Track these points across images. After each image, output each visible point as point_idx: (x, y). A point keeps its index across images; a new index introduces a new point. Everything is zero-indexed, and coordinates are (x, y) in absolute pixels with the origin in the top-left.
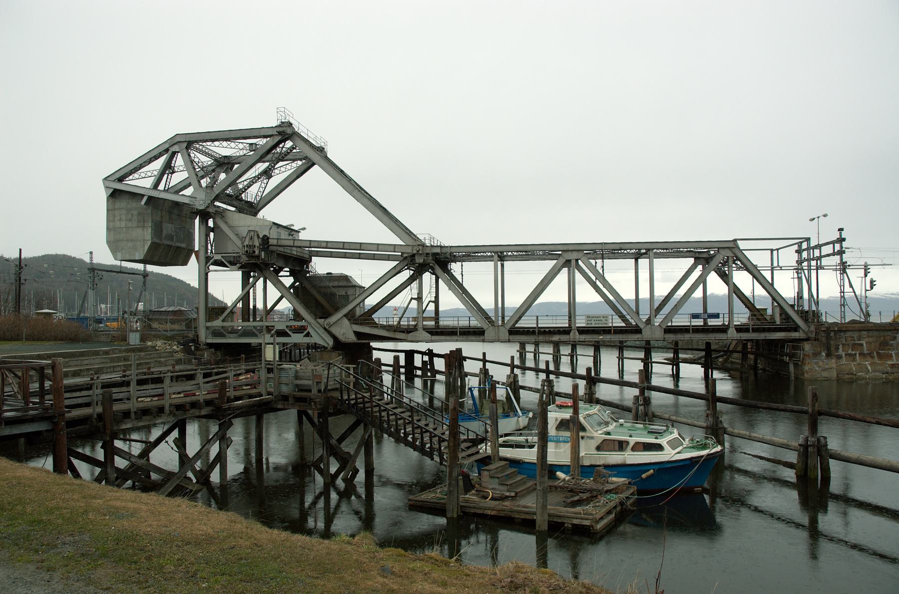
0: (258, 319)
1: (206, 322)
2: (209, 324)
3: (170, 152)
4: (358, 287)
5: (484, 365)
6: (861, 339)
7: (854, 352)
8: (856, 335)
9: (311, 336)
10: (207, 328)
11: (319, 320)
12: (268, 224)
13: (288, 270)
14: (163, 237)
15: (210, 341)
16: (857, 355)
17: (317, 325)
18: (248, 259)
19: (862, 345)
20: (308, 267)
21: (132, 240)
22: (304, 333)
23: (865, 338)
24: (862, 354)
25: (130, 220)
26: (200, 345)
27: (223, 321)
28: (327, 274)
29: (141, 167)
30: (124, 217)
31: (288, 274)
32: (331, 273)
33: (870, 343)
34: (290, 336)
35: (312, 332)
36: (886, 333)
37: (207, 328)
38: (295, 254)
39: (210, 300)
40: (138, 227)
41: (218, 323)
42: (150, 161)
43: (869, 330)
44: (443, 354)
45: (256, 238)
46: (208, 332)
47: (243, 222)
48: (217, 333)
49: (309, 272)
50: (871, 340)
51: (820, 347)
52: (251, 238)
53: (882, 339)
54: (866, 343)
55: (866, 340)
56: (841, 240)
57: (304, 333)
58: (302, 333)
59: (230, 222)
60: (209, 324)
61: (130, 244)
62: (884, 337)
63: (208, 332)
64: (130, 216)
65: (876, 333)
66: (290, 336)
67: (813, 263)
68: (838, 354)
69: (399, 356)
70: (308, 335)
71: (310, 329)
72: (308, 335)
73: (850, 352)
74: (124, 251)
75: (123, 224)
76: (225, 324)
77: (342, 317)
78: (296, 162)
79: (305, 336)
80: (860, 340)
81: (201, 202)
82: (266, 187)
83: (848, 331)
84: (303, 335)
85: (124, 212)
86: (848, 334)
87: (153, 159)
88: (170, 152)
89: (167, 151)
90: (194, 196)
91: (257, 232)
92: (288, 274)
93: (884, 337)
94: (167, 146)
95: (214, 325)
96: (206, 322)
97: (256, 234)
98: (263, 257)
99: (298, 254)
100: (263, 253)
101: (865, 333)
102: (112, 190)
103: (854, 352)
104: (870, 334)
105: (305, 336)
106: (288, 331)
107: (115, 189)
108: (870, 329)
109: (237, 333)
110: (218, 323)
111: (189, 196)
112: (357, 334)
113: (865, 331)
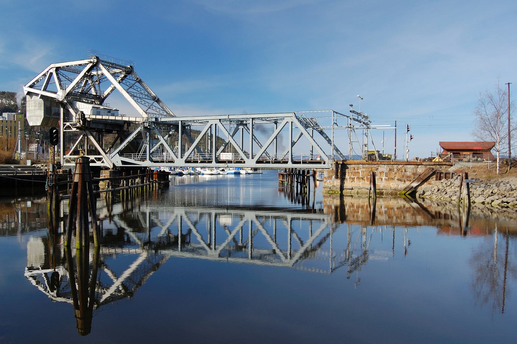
0: (13, 103)
6: (359, 169)
7: (354, 177)
8: (356, 166)
9: (104, 163)
10: (64, 158)
14: (52, 114)
16: (356, 178)
21: (36, 116)
24: (358, 178)
25: (36, 106)
30: (33, 105)
33: (363, 171)
34: (96, 163)
35: (105, 161)
39: (151, 220)
50: (364, 170)
51: (332, 173)
54: (361, 171)
55: (361, 170)
61: (35, 118)
64: (35, 104)
66: (96, 163)
69: (122, 164)
70: (103, 162)
72: (103, 162)
74: (33, 121)
75: (33, 108)
80: (358, 170)
82: (130, 80)
93: (371, 168)
101: (361, 165)
102: (55, 68)
103: (354, 177)
107: (28, 91)
112: (123, 162)
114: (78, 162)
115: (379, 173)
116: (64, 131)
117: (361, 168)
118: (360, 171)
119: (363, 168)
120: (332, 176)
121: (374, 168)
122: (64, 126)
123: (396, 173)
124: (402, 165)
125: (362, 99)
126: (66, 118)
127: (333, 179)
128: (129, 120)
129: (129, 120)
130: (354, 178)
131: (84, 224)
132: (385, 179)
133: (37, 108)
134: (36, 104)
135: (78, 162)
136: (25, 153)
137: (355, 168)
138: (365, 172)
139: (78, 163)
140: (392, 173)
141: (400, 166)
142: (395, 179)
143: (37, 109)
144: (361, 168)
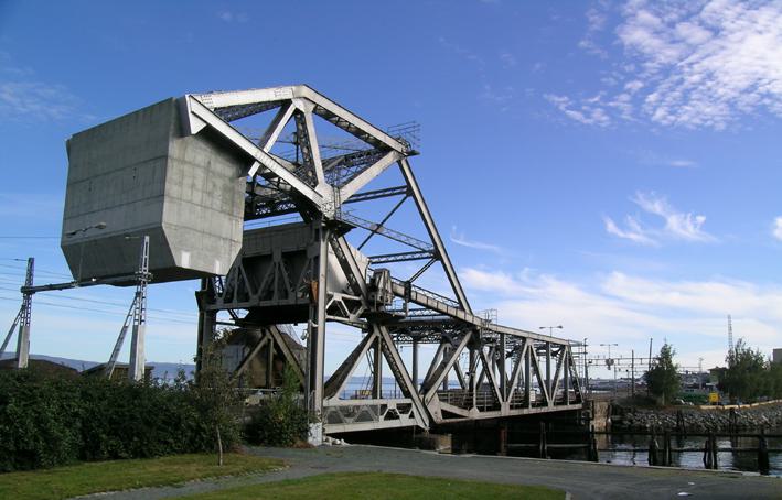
25: (210, 194)
30: (199, 184)
34: (398, 417)
40: (222, 212)
60: (325, 403)
64: (210, 187)
66: (398, 417)
70: (412, 416)
72: (412, 416)
75: (197, 196)
85: (200, 173)
133: (218, 203)
134: (214, 186)
143: (215, 207)
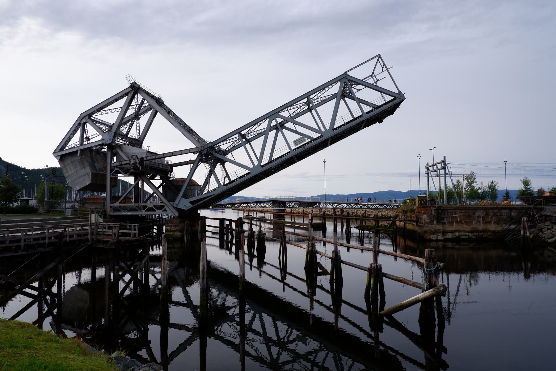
1: (110, 203)
2: (112, 205)
3: (81, 125)
4: (197, 185)
5: (251, 226)
6: (457, 214)
9: (167, 211)
10: (111, 207)
11: (171, 203)
12: (145, 152)
13: (159, 176)
15: (112, 214)
17: (170, 205)
18: (133, 170)
19: (457, 217)
20: (170, 175)
22: (163, 209)
23: (458, 213)
26: (107, 216)
27: (119, 203)
28: (181, 178)
29: (107, 105)
31: (159, 178)
32: (183, 178)
33: (461, 216)
34: (155, 211)
36: (470, 211)
37: (111, 207)
38: (161, 167)
41: (117, 204)
42: (116, 100)
43: (460, 209)
44: (234, 220)
45: (136, 159)
46: (111, 209)
47: (132, 150)
48: (116, 209)
49: (171, 177)
50: (461, 214)
52: (134, 159)
53: (467, 214)
54: (459, 216)
55: (459, 214)
56: (444, 162)
57: (163, 209)
58: (162, 209)
59: (125, 151)
60: (112, 205)
62: (469, 213)
63: (111, 209)
65: (464, 211)
66: (155, 211)
67: (451, 176)
68: (444, 222)
71: (166, 207)
73: (450, 220)
76: (121, 205)
77: (180, 199)
78: (72, 147)
79: (163, 211)
81: (108, 140)
83: (449, 209)
84: (162, 210)
86: (450, 211)
87: (114, 101)
88: (81, 125)
89: (79, 124)
90: (103, 138)
91: (136, 155)
92: (159, 178)
94: (78, 122)
95: (114, 205)
96: (110, 203)
97: (136, 157)
98: (141, 169)
99: (163, 168)
100: (141, 167)
101: (458, 210)
104: (461, 211)
105: (163, 211)
106: (154, 208)
108: (461, 208)
109: (127, 209)
110: (117, 204)
111: (101, 140)
113: (458, 209)
114: (250, 222)
115: (477, 218)
116: (112, 176)
117: (458, 212)
118: (458, 216)
119: (460, 213)
120: (434, 221)
121: (471, 213)
122: (111, 172)
123: (492, 217)
124: (498, 210)
125: (419, 156)
126: (97, 323)
127: (435, 224)
128: (389, 69)
129: (389, 69)
130: (453, 222)
131: (111, 306)
132: (483, 222)
135: (250, 222)
136: (77, 207)
137: (452, 213)
138: (462, 216)
139: (251, 222)
140: (488, 217)
141: (496, 211)
142: (492, 223)
144: (458, 213)
